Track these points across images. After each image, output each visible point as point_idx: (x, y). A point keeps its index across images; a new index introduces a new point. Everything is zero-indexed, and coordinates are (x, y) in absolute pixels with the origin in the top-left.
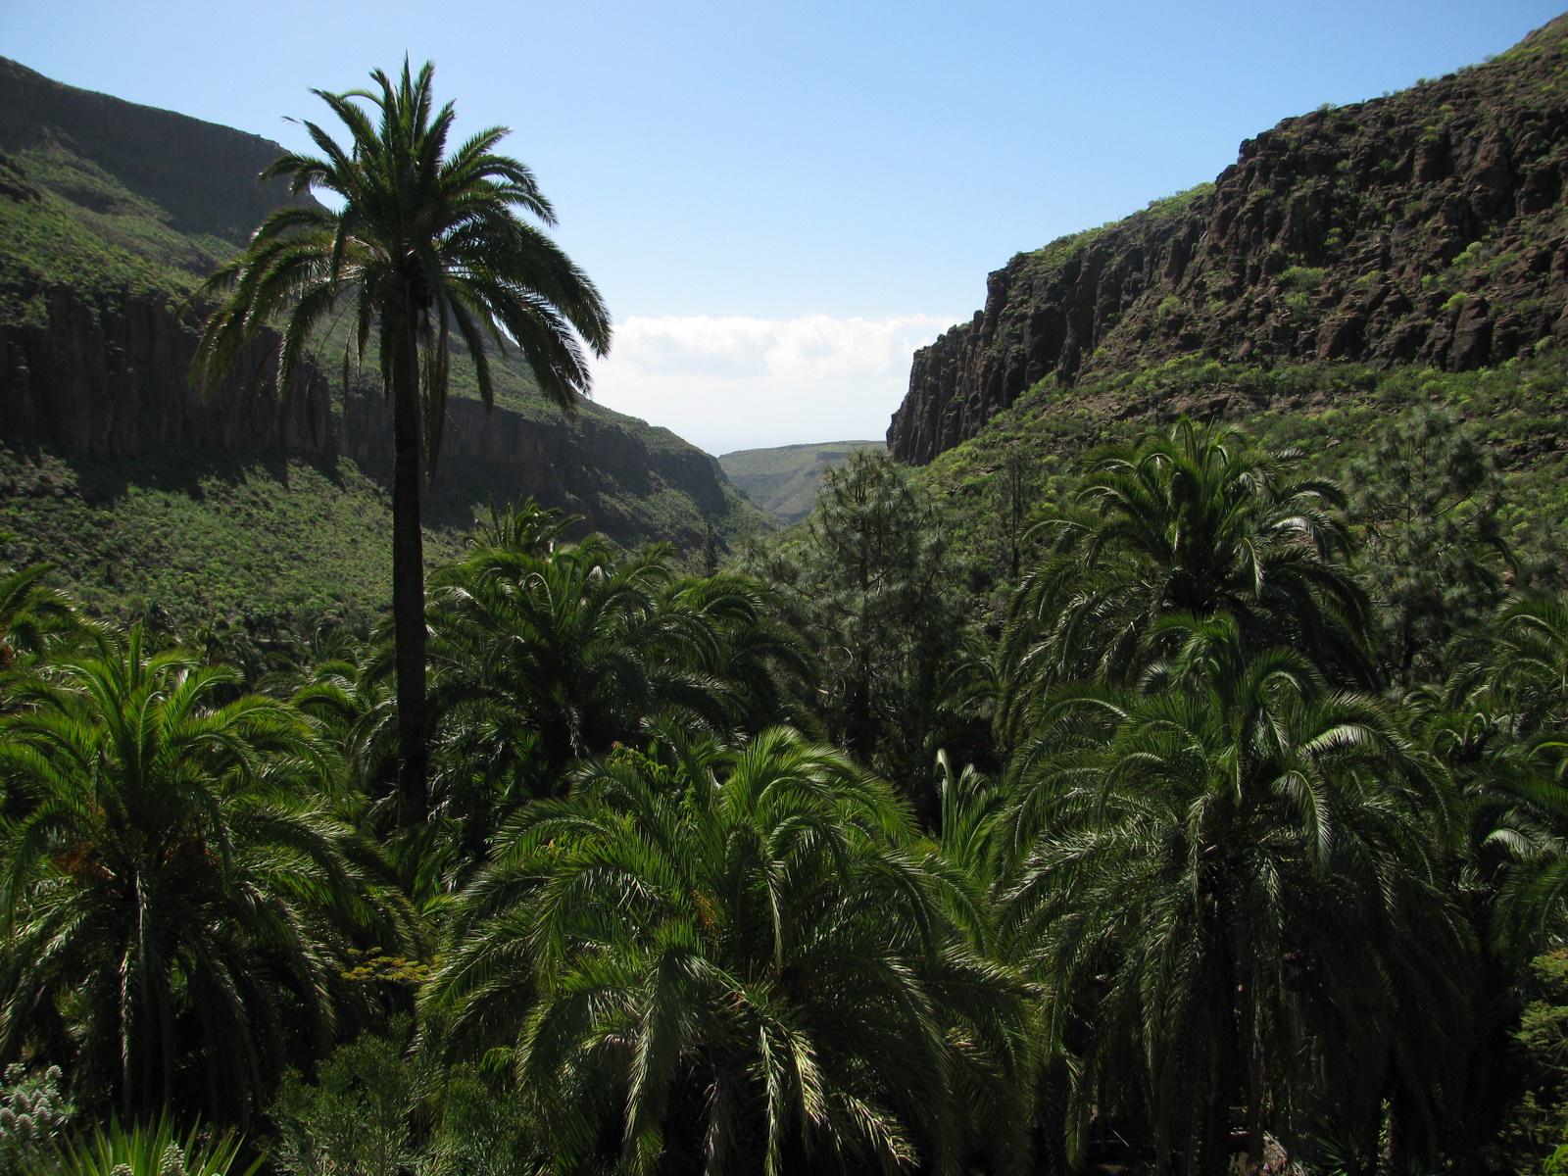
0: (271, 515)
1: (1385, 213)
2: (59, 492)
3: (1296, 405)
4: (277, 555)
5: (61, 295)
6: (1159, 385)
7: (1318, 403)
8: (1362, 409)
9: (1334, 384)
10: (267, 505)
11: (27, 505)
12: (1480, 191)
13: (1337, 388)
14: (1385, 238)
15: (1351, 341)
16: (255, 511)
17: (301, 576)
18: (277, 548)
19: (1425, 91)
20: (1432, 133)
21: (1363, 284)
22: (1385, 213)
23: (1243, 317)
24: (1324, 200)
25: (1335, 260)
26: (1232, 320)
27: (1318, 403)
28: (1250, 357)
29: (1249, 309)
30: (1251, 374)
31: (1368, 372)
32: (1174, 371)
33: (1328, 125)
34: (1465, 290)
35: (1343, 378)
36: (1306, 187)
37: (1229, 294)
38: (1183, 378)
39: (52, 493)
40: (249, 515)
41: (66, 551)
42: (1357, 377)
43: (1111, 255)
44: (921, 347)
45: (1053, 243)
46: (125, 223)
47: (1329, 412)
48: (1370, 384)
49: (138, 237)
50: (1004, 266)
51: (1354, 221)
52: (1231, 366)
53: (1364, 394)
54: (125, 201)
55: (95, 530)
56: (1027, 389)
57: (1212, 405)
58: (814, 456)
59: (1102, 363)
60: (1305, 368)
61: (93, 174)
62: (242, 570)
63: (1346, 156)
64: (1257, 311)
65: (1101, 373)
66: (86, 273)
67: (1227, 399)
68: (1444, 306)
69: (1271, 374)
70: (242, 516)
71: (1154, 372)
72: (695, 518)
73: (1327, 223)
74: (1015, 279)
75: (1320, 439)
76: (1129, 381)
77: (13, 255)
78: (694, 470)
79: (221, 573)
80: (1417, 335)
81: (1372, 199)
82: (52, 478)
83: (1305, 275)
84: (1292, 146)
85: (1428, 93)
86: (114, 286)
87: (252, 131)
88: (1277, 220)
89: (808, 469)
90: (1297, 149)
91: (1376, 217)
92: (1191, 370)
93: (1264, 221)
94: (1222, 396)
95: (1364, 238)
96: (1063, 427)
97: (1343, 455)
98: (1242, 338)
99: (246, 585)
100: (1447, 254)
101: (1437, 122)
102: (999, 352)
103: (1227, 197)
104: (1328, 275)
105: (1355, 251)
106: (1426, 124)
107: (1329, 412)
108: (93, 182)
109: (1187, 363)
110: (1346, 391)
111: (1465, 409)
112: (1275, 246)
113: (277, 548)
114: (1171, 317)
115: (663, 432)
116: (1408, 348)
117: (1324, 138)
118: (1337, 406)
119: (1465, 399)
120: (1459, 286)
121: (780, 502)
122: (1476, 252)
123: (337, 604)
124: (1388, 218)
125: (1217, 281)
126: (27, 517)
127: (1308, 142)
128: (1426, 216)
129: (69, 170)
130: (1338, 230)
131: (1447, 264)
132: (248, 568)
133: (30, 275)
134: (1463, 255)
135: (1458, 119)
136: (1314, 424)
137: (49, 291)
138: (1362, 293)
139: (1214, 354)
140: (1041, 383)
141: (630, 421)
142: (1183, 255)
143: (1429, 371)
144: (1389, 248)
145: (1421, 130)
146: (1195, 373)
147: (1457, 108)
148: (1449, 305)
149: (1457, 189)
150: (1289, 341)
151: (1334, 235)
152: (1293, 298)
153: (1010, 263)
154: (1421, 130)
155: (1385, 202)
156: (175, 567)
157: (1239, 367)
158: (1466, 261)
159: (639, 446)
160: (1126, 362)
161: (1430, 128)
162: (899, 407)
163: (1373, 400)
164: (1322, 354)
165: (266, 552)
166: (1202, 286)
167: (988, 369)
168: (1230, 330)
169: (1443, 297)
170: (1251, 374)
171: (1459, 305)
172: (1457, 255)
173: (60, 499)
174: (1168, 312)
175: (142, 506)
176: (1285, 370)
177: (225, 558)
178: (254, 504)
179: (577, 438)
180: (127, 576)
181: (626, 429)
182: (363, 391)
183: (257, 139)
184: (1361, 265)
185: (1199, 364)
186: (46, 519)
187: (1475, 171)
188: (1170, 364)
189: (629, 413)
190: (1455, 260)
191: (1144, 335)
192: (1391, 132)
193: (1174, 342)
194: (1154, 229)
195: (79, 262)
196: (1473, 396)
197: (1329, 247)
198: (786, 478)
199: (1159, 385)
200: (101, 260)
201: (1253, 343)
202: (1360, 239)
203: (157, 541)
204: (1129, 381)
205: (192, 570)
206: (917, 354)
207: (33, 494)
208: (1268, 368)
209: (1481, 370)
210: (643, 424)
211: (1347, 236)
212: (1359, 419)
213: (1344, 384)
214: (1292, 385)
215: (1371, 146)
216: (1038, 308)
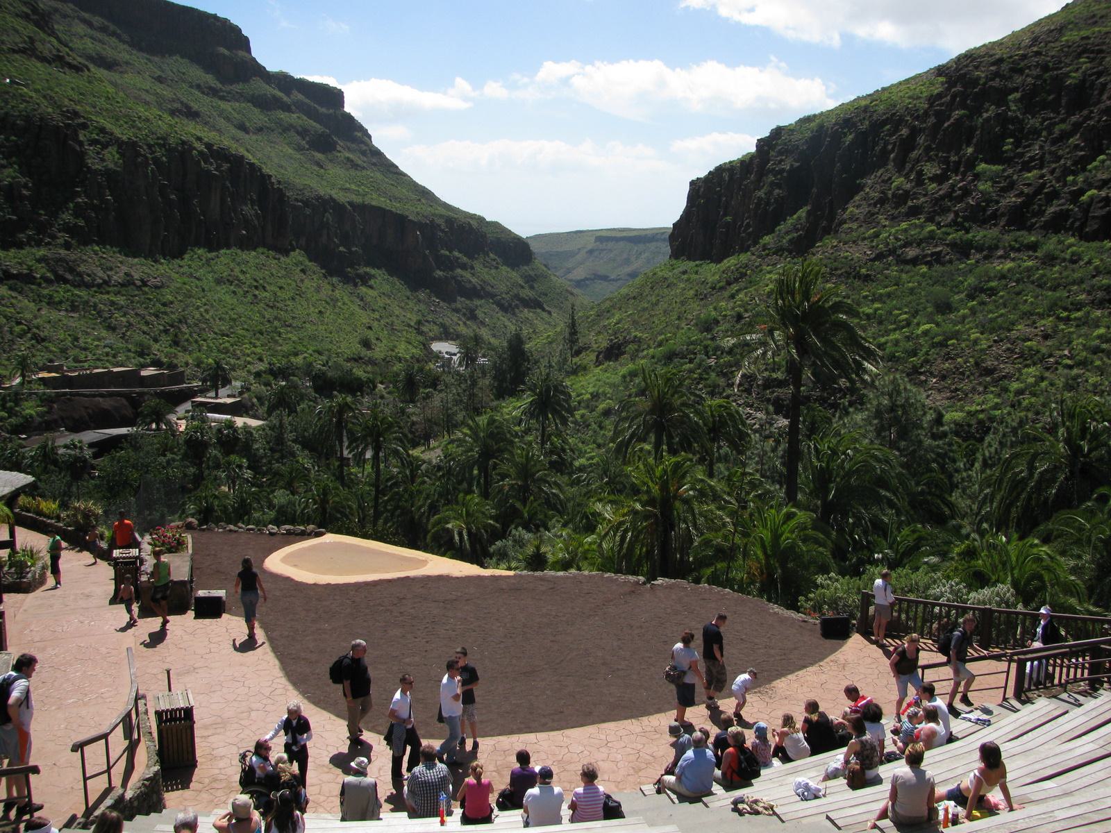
0: (266, 294)
1: (1042, 130)
2: (138, 283)
3: (986, 258)
4: (276, 323)
5: (128, 149)
6: (897, 239)
7: (1000, 257)
8: (1030, 263)
9: (1010, 246)
10: (264, 288)
11: (119, 292)
12: (1106, 121)
13: (1013, 249)
14: (1041, 147)
15: (1019, 218)
16: (257, 292)
17: (294, 338)
18: (276, 318)
19: (1069, 47)
20: (1074, 78)
21: (1028, 178)
22: (1042, 130)
23: (949, 196)
24: (1002, 119)
25: (1008, 161)
26: (942, 198)
27: (1000, 257)
28: (954, 223)
29: (954, 191)
30: (955, 236)
31: (1033, 239)
32: (906, 230)
33: (1005, 67)
34: (1096, 188)
35: (1016, 241)
36: (990, 112)
37: (939, 179)
38: (912, 236)
39: (134, 284)
40: (255, 296)
41: (147, 323)
42: (1026, 242)
43: (845, 135)
44: (695, 178)
45: (800, 120)
46: (130, 79)
47: (1009, 265)
48: (1033, 247)
49: (139, 90)
50: (768, 134)
51: (1023, 136)
52: (943, 229)
53: (1031, 253)
54: (127, 63)
55: (163, 309)
56: (785, 220)
57: (933, 254)
58: (593, 239)
59: (853, 218)
60: (993, 233)
61: (104, 44)
62: (258, 335)
63: (1016, 90)
64: (959, 192)
65: (855, 225)
66: (139, 129)
67: (941, 251)
68: (1082, 198)
69: (970, 236)
70: (250, 298)
71: (893, 231)
72: (522, 287)
73: (1003, 136)
74: (777, 144)
75: (1003, 282)
76: (877, 235)
77: (94, 118)
78: (514, 250)
79: (244, 336)
80: (1062, 216)
81: (1033, 122)
82: (133, 273)
83: (990, 170)
84: (981, 82)
85: (1071, 49)
86: (158, 138)
87: (211, 11)
88: (972, 130)
89: (589, 247)
90: (985, 84)
91: (1036, 133)
92: (918, 230)
93: (962, 134)
94: (939, 249)
95: (1029, 146)
96: (836, 264)
97: (1018, 294)
98: (949, 210)
99: (262, 345)
100: (1081, 164)
101: (1077, 70)
102: (766, 194)
103: (938, 114)
104: (1004, 170)
105: (1022, 155)
106: (1070, 72)
107: (1009, 265)
108: (104, 49)
109: (916, 226)
110: (1018, 250)
111: (1096, 268)
112: (970, 150)
113: (276, 318)
114: (901, 192)
115: (496, 225)
116: (1057, 225)
117: (1002, 77)
118: (1013, 260)
119: (1097, 262)
120: (1090, 186)
121: (569, 271)
122: (1103, 162)
123: (321, 357)
124: (1044, 133)
125: (931, 169)
126: (121, 300)
127: (993, 79)
128: (1070, 134)
129: (88, 41)
130: (1011, 140)
131: (1084, 169)
132: (261, 333)
133: (107, 133)
134: (1095, 164)
135: (1091, 68)
136: (999, 271)
137: (120, 144)
138: (1029, 185)
139: (930, 219)
140: (795, 216)
141: (473, 217)
142: (907, 145)
143: (1072, 240)
144: (1044, 154)
145: (1067, 75)
146: (920, 233)
147: (1092, 60)
148: (1084, 198)
149: (1091, 118)
150: (980, 215)
151: (1008, 144)
152: (982, 186)
153: (771, 133)
154: (1067, 75)
155: (1042, 124)
156: (216, 333)
157: (949, 230)
158: (1095, 168)
159: (484, 236)
160: (870, 219)
161: (1074, 75)
162: (678, 218)
163: (1036, 258)
164: (1002, 224)
165: (269, 321)
166: (920, 174)
167: (758, 205)
168: (938, 207)
169: (1082, 192)
170: (955, 236)
171: (1092, 198)
172: (1090, 163)
173: (139, 288)
174: (898, 188)
175: (189, 291)
176: (979, 234)
177: (246, 327)
178: (256, 288)
179: (443, 231)
180: (187, 340)
181: (474, 224)
182: (301, 201)
183: (215, 17)
184: (1027, 167)
185: (922, 227)
186: (132, 302)
187: (1102, 106)
188: (904, 225)
189: (472, 211)
190: (1089, 167)
191: (882, 201)
192: (1047, 75)
193: (903, 210)
194: (875, 118)
195: (134, 121)
196: (1102, 260)
197: (1006, 152)
198: (572, 254)
199: (897, 239)
200: (147, 120)
201: (956, 214)
202: (1025, 147)
203: (202, 315)
204: (877, 235)
205: (227, 336)
206: (692, 183)
207: (123, 285)
208: (967, 232)
209: (1105, 242)
210: (481, 220)
211: (1017, 144)
212: (1029, 269)
213: (1017, 246)
214: (983, 244)
215: (1034, 84)
216: (792, 165)
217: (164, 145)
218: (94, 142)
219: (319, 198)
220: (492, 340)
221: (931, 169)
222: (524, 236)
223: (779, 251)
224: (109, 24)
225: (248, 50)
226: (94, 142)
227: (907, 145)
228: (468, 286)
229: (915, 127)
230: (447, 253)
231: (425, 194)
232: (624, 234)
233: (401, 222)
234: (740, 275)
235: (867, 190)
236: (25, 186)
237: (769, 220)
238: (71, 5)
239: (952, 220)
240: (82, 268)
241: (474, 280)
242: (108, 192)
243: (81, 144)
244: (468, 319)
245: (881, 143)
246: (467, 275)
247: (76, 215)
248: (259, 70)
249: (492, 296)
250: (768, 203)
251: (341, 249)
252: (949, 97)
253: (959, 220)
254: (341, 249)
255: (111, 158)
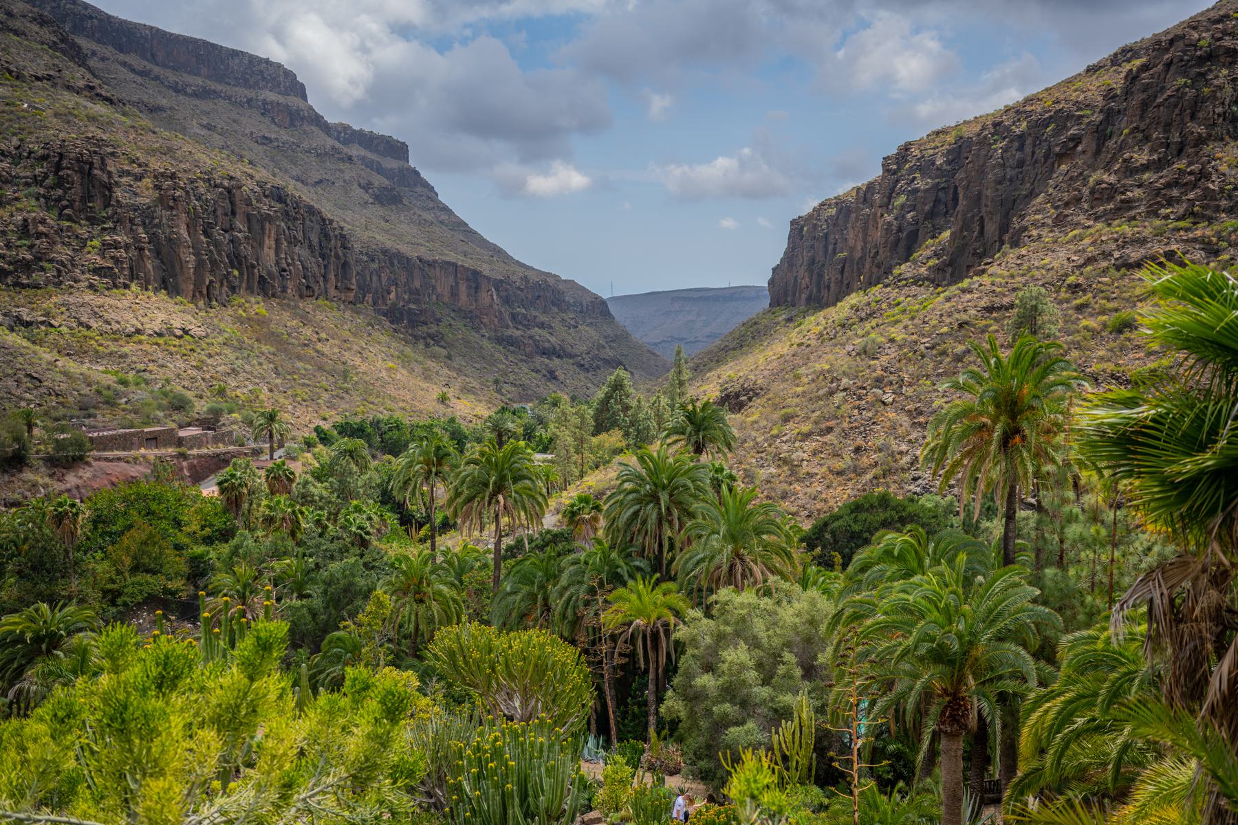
2: (179, 333)
23: (1174, 184)
78: (598, 309)
206: (793, 222)
217: (209, 180)
218: (123, 173)
219: (385, 252)
220: (325, 642)
221: (1141, 157)
222: (605, 296)
223: (917, 281)
224: (152, 66)
225: (304, 97)
226: (123, 173)
227: (1101, 133)
228: (547, 345)
229: (1111, 109)
230: (523, 311)
231: (498, 252)
232: (710, 294)
233: (475, 279)
234: (867, 314)
235: (1051, 190)
236: (43, 222)
237: (905, 243)
238: (110, 48)
239: (1186, 210)
240: (111, 315)
241: (553, 339)
242: (141, 230)
243: (110, 174)
244: (549, 380)
245: (1045, 146)
246: (545, 333)
247: (102, 254)
248: (318, 120)
249: (571, 356)
250: (900, 229)
251: (412, 306)
252: (1160, 67)
253: (1196, 209)
254: (412, 306)
255: (146, 194)
